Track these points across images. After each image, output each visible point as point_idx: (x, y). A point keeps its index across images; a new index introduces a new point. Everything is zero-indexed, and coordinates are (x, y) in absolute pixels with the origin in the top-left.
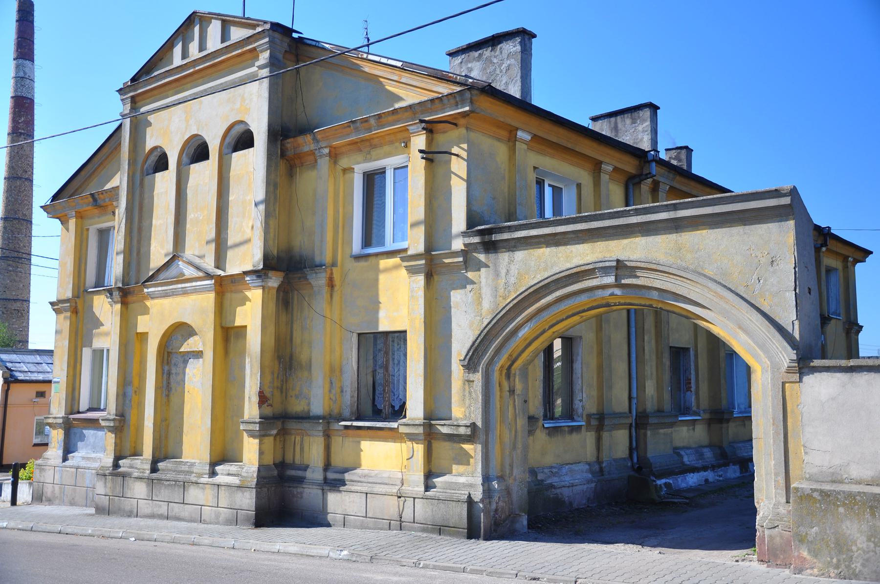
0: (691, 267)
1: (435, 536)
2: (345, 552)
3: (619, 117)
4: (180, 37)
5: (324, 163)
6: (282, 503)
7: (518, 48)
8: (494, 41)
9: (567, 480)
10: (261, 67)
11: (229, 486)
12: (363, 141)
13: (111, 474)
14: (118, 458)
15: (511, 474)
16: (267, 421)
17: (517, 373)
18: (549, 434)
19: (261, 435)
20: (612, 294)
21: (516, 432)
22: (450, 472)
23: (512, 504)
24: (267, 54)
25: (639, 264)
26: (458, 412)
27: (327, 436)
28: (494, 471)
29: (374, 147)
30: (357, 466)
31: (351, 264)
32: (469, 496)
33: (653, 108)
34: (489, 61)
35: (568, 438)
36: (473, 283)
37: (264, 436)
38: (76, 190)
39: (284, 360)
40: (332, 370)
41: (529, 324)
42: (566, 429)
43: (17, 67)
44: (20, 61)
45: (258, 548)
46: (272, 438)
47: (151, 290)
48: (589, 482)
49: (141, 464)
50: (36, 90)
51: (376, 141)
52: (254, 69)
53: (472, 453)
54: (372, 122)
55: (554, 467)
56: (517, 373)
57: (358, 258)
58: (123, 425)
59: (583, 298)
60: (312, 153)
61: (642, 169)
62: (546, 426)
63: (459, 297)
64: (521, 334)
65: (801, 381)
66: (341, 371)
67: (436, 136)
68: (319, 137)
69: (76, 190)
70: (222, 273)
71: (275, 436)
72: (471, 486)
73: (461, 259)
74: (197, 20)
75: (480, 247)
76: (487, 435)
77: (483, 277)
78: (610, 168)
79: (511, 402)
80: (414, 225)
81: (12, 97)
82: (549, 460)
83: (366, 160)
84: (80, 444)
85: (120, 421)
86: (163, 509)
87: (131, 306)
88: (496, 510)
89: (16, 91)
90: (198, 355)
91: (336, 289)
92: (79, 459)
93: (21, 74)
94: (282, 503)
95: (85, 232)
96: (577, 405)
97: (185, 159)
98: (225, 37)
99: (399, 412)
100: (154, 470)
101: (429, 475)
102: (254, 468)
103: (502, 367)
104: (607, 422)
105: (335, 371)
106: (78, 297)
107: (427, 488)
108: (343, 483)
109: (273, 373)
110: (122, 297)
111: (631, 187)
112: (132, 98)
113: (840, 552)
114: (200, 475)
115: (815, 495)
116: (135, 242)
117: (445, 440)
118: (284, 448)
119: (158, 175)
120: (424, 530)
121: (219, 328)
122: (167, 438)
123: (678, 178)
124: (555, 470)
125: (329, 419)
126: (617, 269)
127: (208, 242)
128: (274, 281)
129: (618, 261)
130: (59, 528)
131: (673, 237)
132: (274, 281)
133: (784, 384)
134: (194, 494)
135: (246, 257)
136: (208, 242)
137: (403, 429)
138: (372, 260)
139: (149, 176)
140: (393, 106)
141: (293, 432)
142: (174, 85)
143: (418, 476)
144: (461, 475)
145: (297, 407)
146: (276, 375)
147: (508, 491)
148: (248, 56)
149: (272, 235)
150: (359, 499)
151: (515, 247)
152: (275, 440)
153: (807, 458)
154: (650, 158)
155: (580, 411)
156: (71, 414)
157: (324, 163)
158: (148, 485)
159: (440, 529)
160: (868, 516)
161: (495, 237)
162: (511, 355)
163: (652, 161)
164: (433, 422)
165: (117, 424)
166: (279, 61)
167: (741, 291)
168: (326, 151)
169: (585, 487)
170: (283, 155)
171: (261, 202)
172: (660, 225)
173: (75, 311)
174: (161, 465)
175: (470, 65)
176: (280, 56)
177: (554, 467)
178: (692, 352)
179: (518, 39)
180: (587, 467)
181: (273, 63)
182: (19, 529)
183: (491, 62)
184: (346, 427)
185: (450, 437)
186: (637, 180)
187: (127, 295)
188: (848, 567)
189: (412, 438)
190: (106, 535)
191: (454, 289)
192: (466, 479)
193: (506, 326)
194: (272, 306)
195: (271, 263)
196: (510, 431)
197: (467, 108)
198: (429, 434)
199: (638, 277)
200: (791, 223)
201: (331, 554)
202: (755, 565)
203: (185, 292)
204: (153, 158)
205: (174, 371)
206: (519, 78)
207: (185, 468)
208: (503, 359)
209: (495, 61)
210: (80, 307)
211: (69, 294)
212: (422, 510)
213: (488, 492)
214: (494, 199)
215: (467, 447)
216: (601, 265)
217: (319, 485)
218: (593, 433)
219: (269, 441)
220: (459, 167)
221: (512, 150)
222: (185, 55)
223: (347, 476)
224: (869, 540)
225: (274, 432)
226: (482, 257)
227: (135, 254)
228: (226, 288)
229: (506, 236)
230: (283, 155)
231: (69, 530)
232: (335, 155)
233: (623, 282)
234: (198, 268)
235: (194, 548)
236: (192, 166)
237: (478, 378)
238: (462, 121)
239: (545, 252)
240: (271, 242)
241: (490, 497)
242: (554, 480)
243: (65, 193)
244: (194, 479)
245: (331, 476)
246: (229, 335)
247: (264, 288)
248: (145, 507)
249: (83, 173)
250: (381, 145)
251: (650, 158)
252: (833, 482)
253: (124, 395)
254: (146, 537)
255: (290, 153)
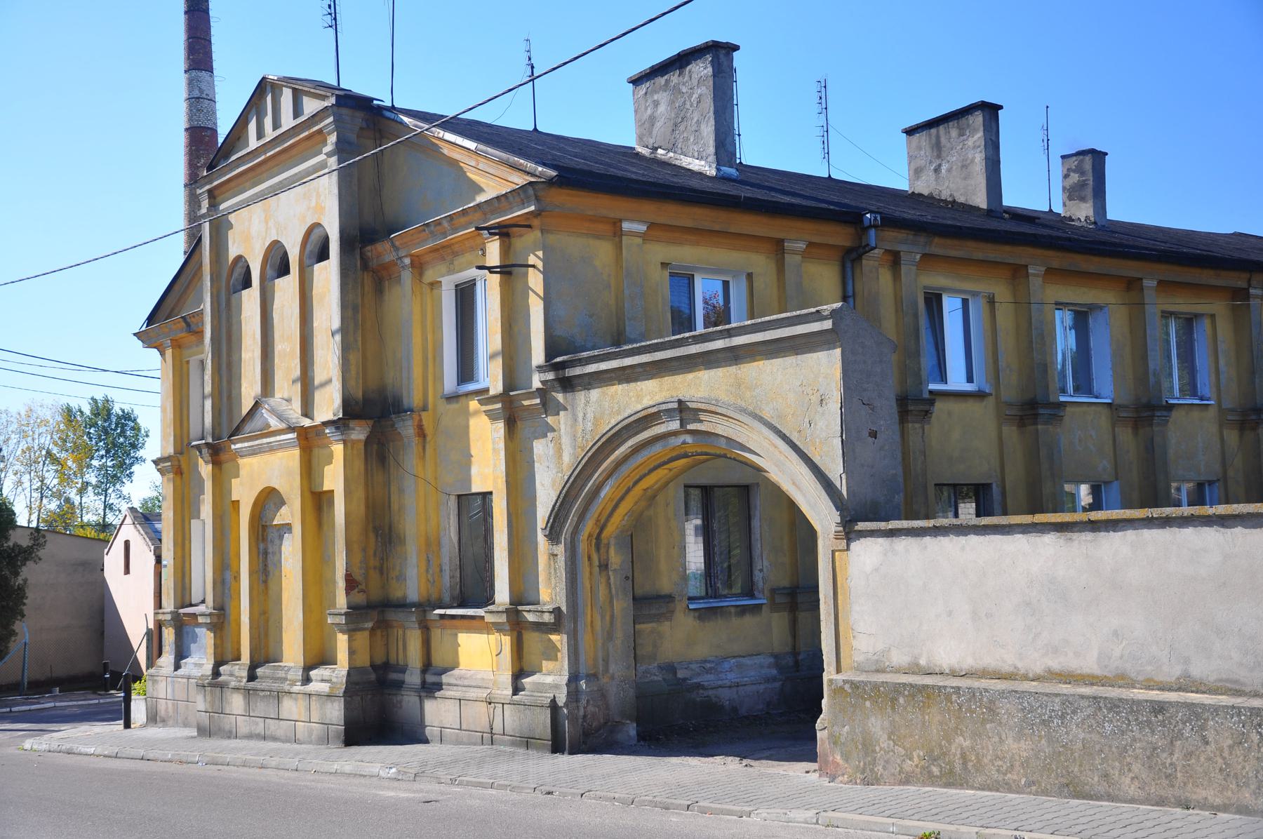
0: (751, 408)
1: (522, 751)
2: (394, 770)
3: (941, 127)
4: (254, 110)
5: (407, 276)
6: (379, 714)
7: (710, 69)
8: (681, 61)
9: (732, 677)
10: (329, 155)
11: (319, 695)
12: (443, 247)
13: (210, 685)
14: (218, 664)
15: (606, 670)
16: (356, 613)
17: (612, 542)
18: (700, 618)
19: (351, 627)
20: (684, 443)
21: (612, 616)
22: (540, 671)
23: (607, 708)
24: (333, 138)
25: (702, 406)
26: (545, 594)
27: (425, 628)
28: (583, 670)
29: (456, 254)
30: (455, 665)
31: (443, 407)
32: (554, 701)
33: (990, 110)
34: (676, 90)
35: (736, 622)
36: (554, 430)
37: (354, 630)
38: (173, 309)
39: (379, 530)
40: (428, 543)
41: (610, 482)
42: (733, 610)
43: (191, 83)
44: (194, 73)
45: (318, 769)
46: (366, 633)
47: (238, 446)
48: (768, 680)
49: (236, 672)
50: (219, 114)
51: (456, 248)
52: (322, 157)
53: (558, 645)
54: (446, 224)
55: (709, 662)
56: (612, 542)
57: (453, 398)
58: (221, 621)
59: (657, 448)
60: (393, 263)
61: (861, 239)
62: (691, 607)
63: (540, 447)
64: (603, 494)
65: (848, 549)
66: (439, 544)
67: (514, 240)
68: (397, 243)
69: (173, 309)
70: (307, 423)
71: (372, 630)
72: (556, 686)
73: (538, 401)
74: (269, 88)
75: (557, 385)
76: (575, 623)
77: (561, 421)
78: (802, 246)
79: (603, 580)
80: (492, 357)
81: (187, 130)
82: (701, 651)
83: (451, 272)
84: (193, 646)
85: (219, 616)
86: (260, 729)
87: (225, 466)
88: (585, 716)
89: (190, 119)
90: (288, 527)
91: (428, 439)
92: (192, 667)
93: (196, 93)
94: (379, 714)
95: (185, 366)
96: (758, 576)
97: (270, 272)
98: (297, 112)
99: (486, 598)
100: (252, 677)
101: (519, 674)
102: (344, 672)
103: (590, 535)
104: (800, 599)
105: (432, 545)
106: (181, 453)
107: (516, 690)
108: (439, 686)
109: (364, 550)
110: (211, 455)
111: (849, 265)
112: (210, 191)
113: (866, 754)
114: (293, 683)
115: (847, 687)
116: (225, 383)
117: (534, 630)
118: (387, 645)
119: (245, 292)
120: (513, 744)
121: (307, 494)
122: (266, 635)
123: (937, 240)
124: (705, 666)
125: (424, 606)
126: (681, 412)
127: (294, 382)
128: (359, 433)
129: (680, 402)
130: (141, 752)
131: (732, 369)
132: (359, 433)
133: (833, 552)
134: (290, 708)
135: (328, 405)
136: (294, 382)
137: (489, 619)
138: (463, 400)
139: (236, 295)
140: (474, 200)
141: (395, 624)
142: (250, 175)
143: (506, 677)
144: (549, 674)
145: (396, 594)
146: (371, 552)
147: (602, 694)
148: (318, 138)
149: (353, 373)
150: (452, 706)
151: (589, 384)
152: (371, 636)
153: (855, 643)
154: (866, 223)
155: (760, 584)
156: (183, 607)
157: (407, 276)
158: (245, 697)
159: (527, 742)
160: (889, 710)
161: (571, 372)
162: (598, 521)
163: (871, 226)
164: (520, 608)
165: (215, 620)
166: (350, 143)
167: (795, 438)
168: (407, 261)
169: (762, 687)
170: (365, 266)
171: (337, 332)
172: (719, 355)
173: (179, 472)
174: (260, 671)
175: (656, 97)
176: (353, 137)
177: (709, 662)
178: (995, 489)
179: (709, 58)
180: (772, 660)
181: (343, 149)
182: (105, 756)
183: (680, 92)
184: (442, 616)
185: (539, 626)
186: (854, 255)
187: (217, 453)
188: (871, 770)
189: (498, 628)
190: (184, 759)
191: (537, 438)
192: (552, 678)
193: (584, 485)
194: (359, 465)
195: (352, 410)
196: (603, 618)
197: (533, 208)
198: (515, 624)
199: (701, 421)
200: (838, 351)
201: (381, 773)
202: (814, 777)
203: (271, 449)
204: (239, 271)
205: (270, 550)
206: (711, 114)
207: (281, 674)
208: (589, 527)
209: (684, 90)
210: (184, 466)
211: (170, 450)
212: (509, 720)
213: (574, 694)
214: (591, 316)
215: (554, 637)
216: (664, 407)
217: (416, 690)
218: (786, 614)
219: (363, 638)
220: (535, 280)
221: (619, 247)
222: (260, 135)
223: (445, 679)
224: (889, 738)
225: (370, 625)
226: (560, 397)
227: (225, 399)
228: (309, 440)
229: (578, 371)
230: (365, 266)
231: (151, 756)
232: (418, 266)
233: (690, 427)
234: (280, 418)
235: (263, 771)
236: (277, 281)
237: (560, 549)
238: (536, 222)
239: (618, 390)
240: (353, 383)
241: (577, 701)
242: (707, 679)
243: (161, 314)
244: (287, 688)
245: (430, 678)
246: (318, 501)
247: (345, 442)
248: (243, 725)
249: (176, 287)
250: (463, 253)
251: (866, 223)
252: (877, 671)
253: (223, 582)
254: (220, 761)
255: (373, 264)
